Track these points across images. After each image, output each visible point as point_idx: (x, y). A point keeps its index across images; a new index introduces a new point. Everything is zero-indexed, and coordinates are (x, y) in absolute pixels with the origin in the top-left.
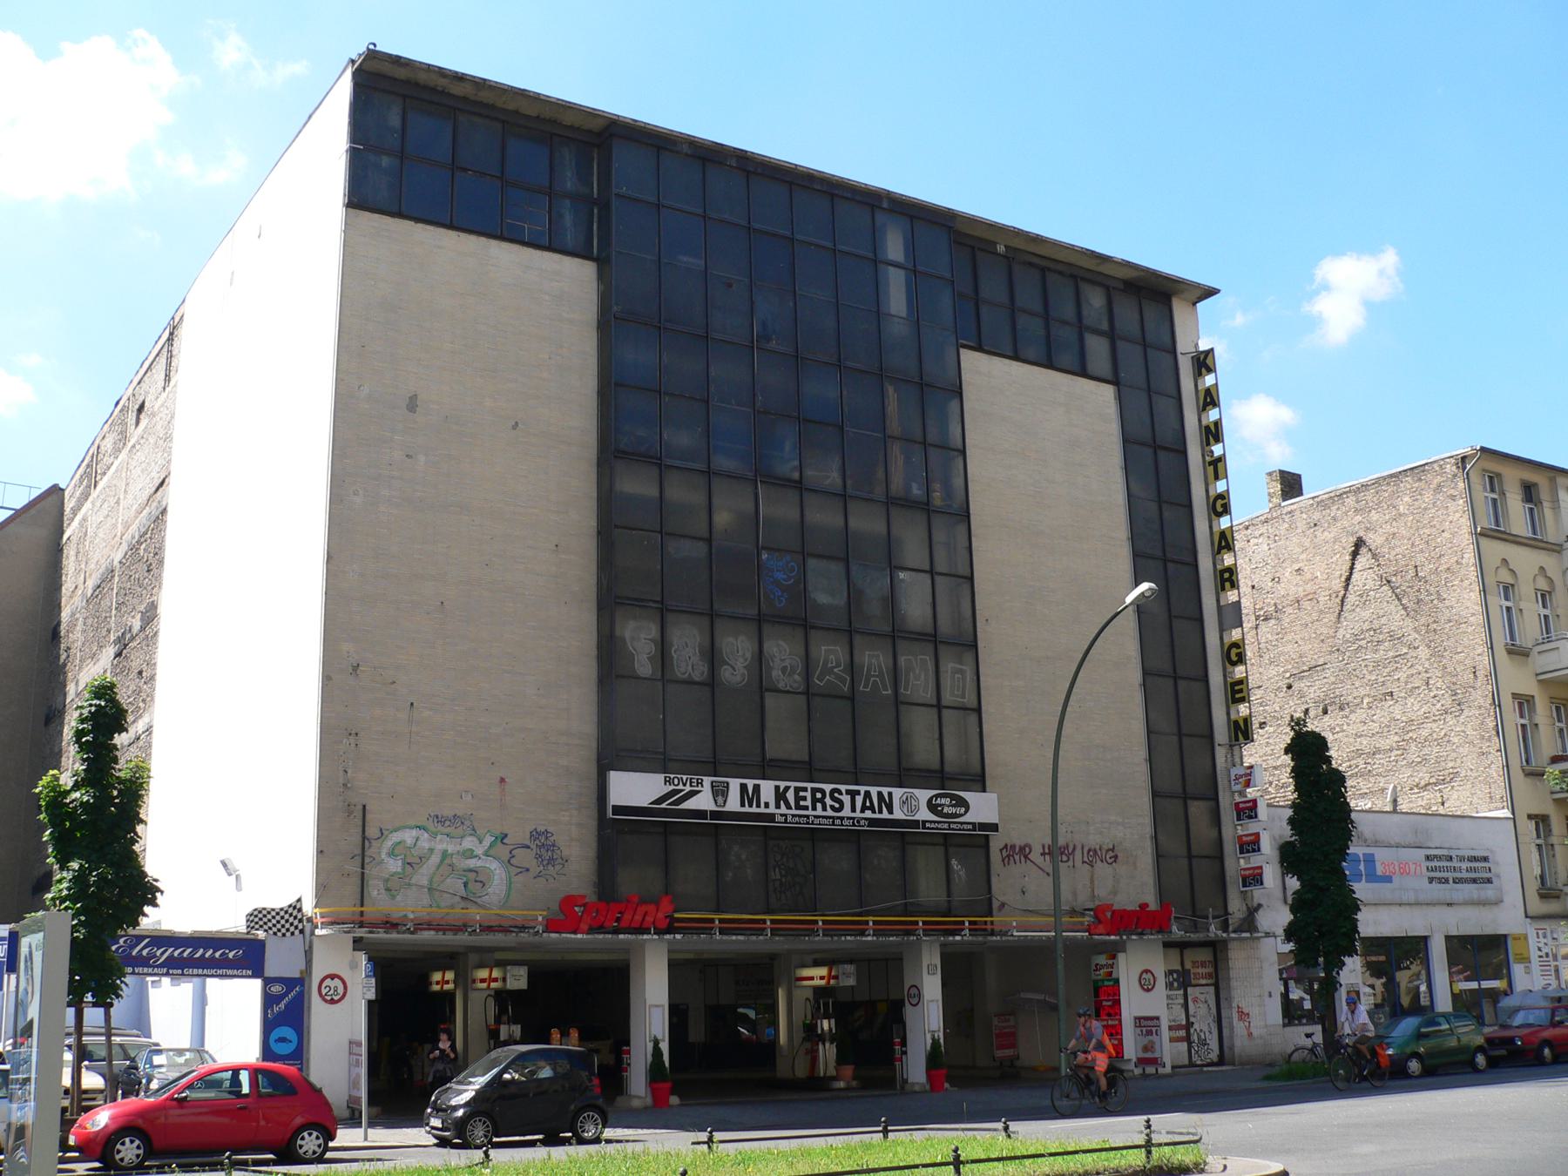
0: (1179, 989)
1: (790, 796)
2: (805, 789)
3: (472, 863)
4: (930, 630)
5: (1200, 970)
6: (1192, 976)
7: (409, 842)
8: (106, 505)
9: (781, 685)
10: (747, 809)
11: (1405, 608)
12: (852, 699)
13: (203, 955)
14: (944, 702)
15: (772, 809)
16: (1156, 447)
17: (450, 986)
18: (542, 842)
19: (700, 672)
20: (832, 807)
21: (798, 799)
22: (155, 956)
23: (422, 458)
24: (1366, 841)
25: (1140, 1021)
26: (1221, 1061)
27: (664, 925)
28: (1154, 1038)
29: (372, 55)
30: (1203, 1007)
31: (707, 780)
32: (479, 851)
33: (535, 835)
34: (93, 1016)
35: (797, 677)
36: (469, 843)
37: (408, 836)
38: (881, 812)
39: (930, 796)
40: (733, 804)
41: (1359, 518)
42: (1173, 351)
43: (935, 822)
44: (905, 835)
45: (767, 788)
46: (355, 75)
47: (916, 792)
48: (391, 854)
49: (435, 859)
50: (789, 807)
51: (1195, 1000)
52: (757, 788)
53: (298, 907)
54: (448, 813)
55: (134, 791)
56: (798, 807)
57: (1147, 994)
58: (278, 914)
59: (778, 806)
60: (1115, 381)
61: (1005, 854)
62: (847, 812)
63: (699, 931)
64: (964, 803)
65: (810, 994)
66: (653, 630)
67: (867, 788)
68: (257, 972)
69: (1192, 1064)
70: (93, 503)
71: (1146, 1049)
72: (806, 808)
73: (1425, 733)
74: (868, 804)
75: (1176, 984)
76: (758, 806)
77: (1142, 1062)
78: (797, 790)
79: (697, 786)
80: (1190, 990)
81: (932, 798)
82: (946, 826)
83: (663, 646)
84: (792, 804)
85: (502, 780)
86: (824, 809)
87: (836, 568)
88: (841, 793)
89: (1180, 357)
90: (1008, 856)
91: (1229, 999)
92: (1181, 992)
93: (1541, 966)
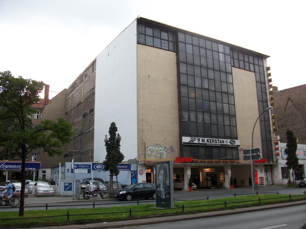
1: (209, 140)
3: (161, 152)
4: (228, 113)
5: (269, 169)
7: (152, 148)
8: (78, 92)
9: (207, 123)
10: (203, 143)
11: (297, 109)
12: (217, 125)
14: (231, 125)
15: (206, 143)
16: (261, 83)
17: (150, 172)
18: (171, 148)
19: (195, 120)
21: (210, 141)
23: (151, 85)
25: (260, 178)
26: (272, 185)
27: (191, 162)
28: (263, 181)
29: (141, 18)
30: (270, 176)
31: (197, 138)
32: (162, 150)
33: (170, 147)
34: (114, 177)
36: (161, 148)
37: (151, 147)
40: (201, 142)
41: (289, 94)
42: (263, 66)
44: (226, 147)
45: (206, 139)
46: (137, 21)
48: (149, 150)
49: (156, 151)
54: (157, 143)
55: (118, 140)
56: (210, 142)
59: (207, 142)
60: (255, 72)
62: (217, 143)
64: (234, 142)
65: (205, 173)
66: (187, 114)
68: (130, 170)
69: (268, 185)
70: (75, 92)
71: (261, 182)
73: (301, 131)
77: (260, 184)
78: (210, 140)
83: (189, 116)
85: (165, 138)
87: (214, 103)
89: (264, 68)
91: (274, 174)
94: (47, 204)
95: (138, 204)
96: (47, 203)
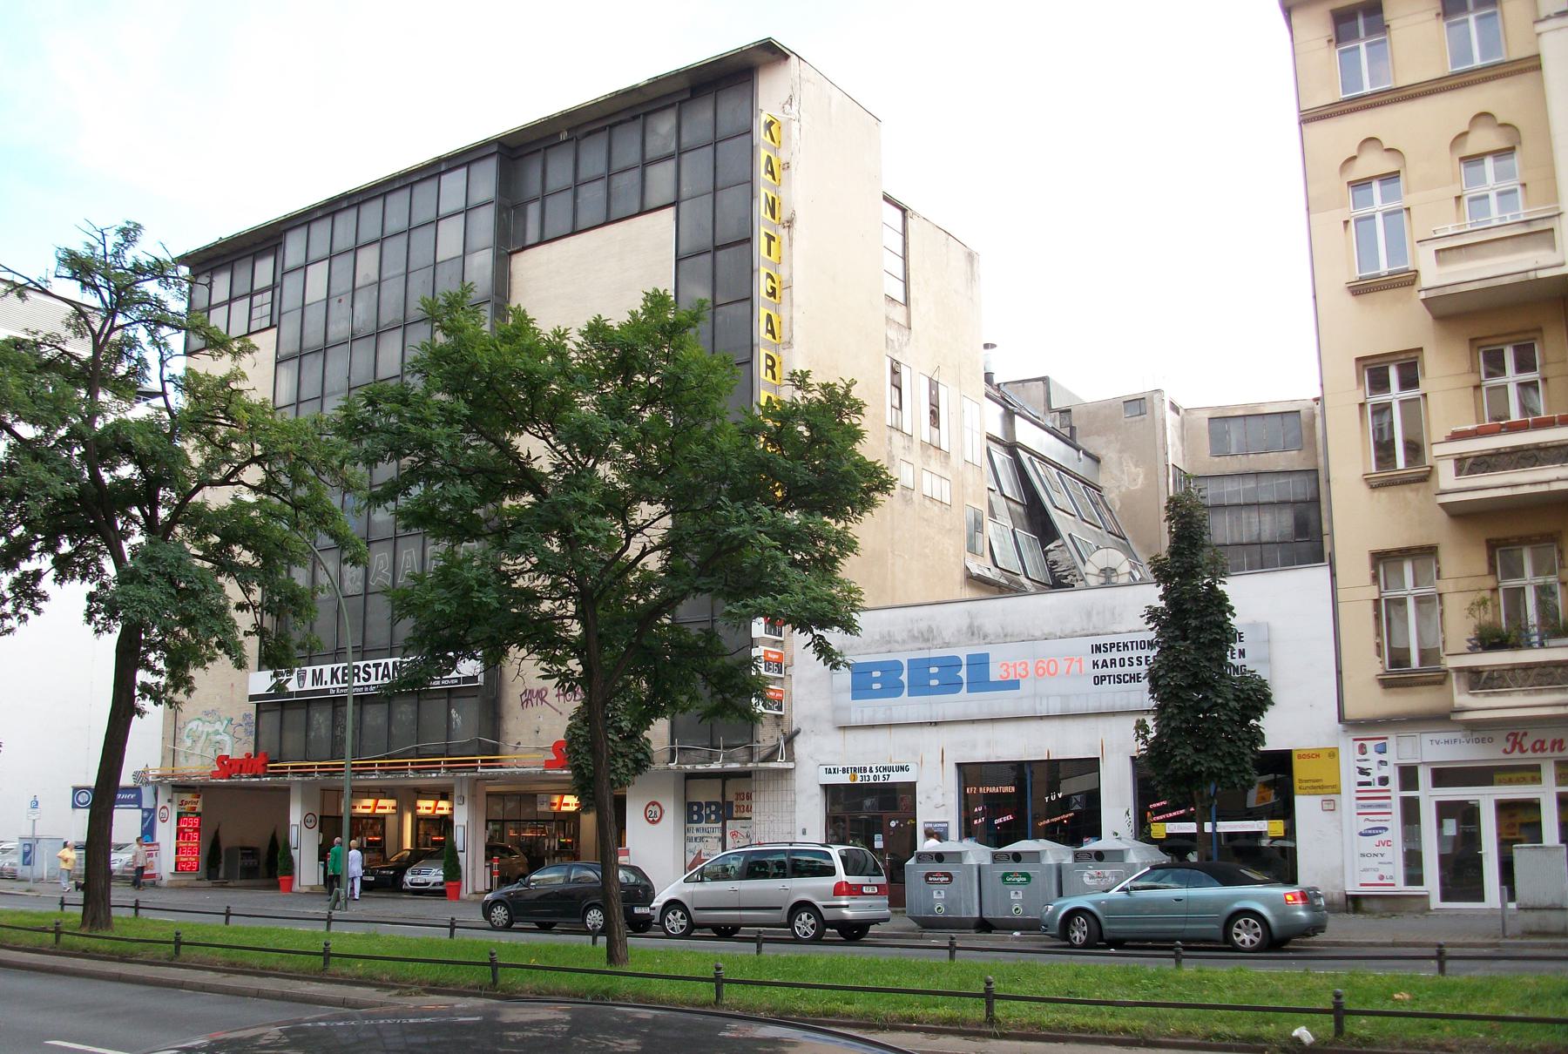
0: (716, 821)
1: (340, 674)
3: (218, 738)
6: (735, 809)
15: (329, 686)
24: (985, 637)
32: (221, 731)
35: (359, 583)
36: (218, 726)
40: (308, 686)
48: (188, 737)
49: (204, 736)
50: (338, 683)
51: (734, 834)
56: (344, 682)
57: (652, 826)
59: (332, 683)
61: (524, 698)
62: (372, 681)
63: (305, 774)
75: (713, 817)
80: (729, 823)
85: (232, 685)
88: (369, 667)
90: (527, 700)
92: (720, 825)
93: (1359, 799)
94: (1440, 946)
95: (227, 922)
96: (1441, 941)
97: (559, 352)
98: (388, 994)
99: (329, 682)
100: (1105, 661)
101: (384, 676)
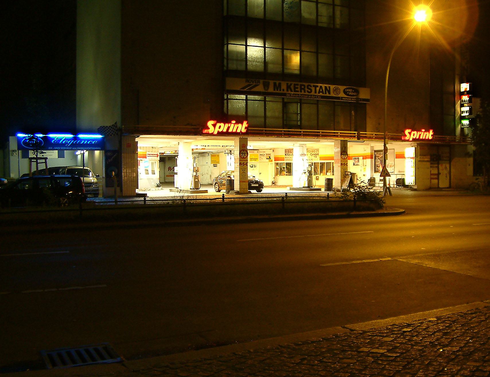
1: (292, 87)
2: (297, 85)
10: (276, 91)
13: (84, 142)
15: (285, 92)
20: (308, 91)
21: (295, 88)
22: (67, 143)
38: (326, 93)
39: (344, 89)
43: (346, 98)
47: (340, 87)
52: (280, 84)
53: (116, 126)
56: (295, 91)
58: (109, 128)
59: (287, 91)
62: (313, 93)
67: (321, 85)
72: (298, 91)
74: (321, 91)
76: (280, 90)
78: (295, 85)
79: (258, 83)
81: (345, 89)
82: (350, 99)
84: (293, 90)
86: (305, 92)
97: (419, 28)
98: (250, 178)
99: (285, 90)
100: (466, 113)
101: (319, 92)
